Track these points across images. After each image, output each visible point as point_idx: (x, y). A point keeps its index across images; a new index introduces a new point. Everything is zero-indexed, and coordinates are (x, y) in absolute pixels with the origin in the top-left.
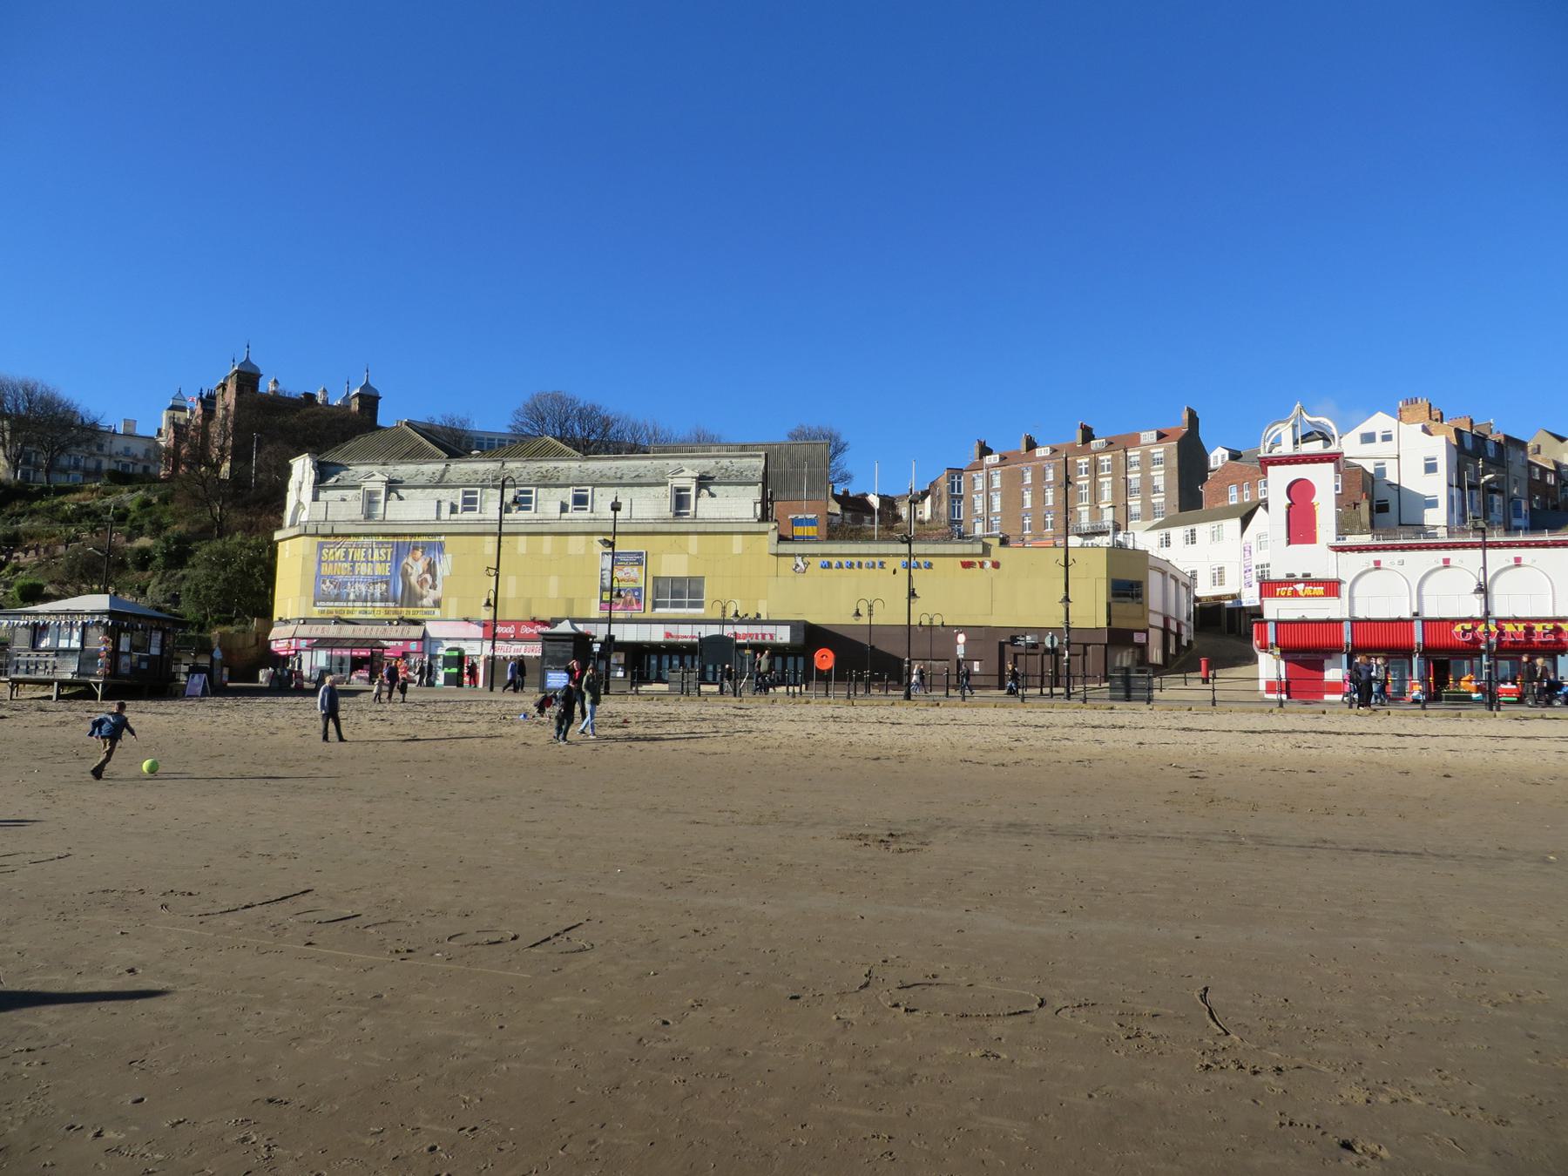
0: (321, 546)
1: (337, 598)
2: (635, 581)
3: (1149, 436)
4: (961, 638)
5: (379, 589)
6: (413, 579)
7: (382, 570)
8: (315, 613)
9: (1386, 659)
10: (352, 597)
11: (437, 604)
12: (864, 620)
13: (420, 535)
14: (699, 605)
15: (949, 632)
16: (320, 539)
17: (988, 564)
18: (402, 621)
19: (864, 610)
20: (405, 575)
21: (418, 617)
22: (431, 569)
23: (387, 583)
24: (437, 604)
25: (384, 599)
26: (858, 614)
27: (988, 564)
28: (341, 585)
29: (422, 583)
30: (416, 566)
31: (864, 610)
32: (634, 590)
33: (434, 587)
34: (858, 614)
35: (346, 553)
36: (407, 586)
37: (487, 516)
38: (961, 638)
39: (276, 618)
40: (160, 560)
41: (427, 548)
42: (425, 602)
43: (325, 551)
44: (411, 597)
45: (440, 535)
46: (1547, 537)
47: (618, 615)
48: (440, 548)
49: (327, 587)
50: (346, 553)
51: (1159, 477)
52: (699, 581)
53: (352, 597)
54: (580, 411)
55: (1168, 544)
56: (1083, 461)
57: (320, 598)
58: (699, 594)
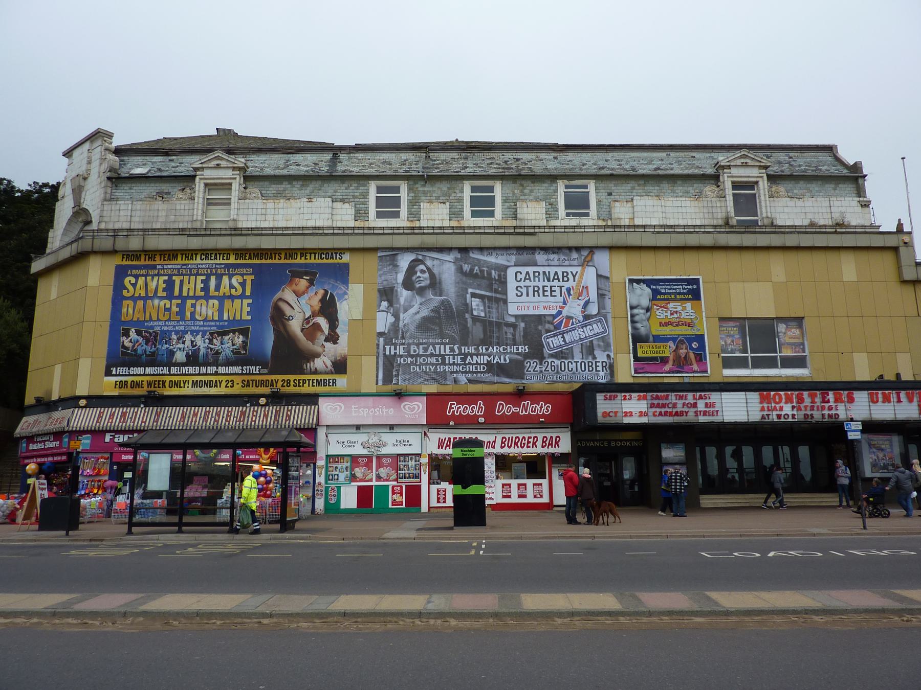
0: (121, 273)
1: (152, 360)
2: (689, 325)
4: (695, 287)
5: (230, 344)
6: (295, 326)
7: (241, 310)
8: (108, 385)
10: (180, 357)
11: (340, 366)
13: (304, 252)
16: (118, 260)
18: (277, 398)
20: (279, 318)
21: (306, 389)
22: (328, 308)
23: (244, 332)
24: (340, 366)
25: (239, 359)
28: (152, 338)
29: (312, 331)
30: (299, 304)
32: (690, 339)
33: (333, 338)
35: (170, 285)
36: (284, 339)
38: (695, 287)
39: (29, 400)
41: (311, 274)
42: (318, 363)
43: (128, 280)
44: (290, 356)
45: (341, 251)
46: (381, 363)
47: (186, 519)
48: (341, 273)
49: (131, 340)
50: (170, 285)
53: (180, 357)
57: (118, 359)
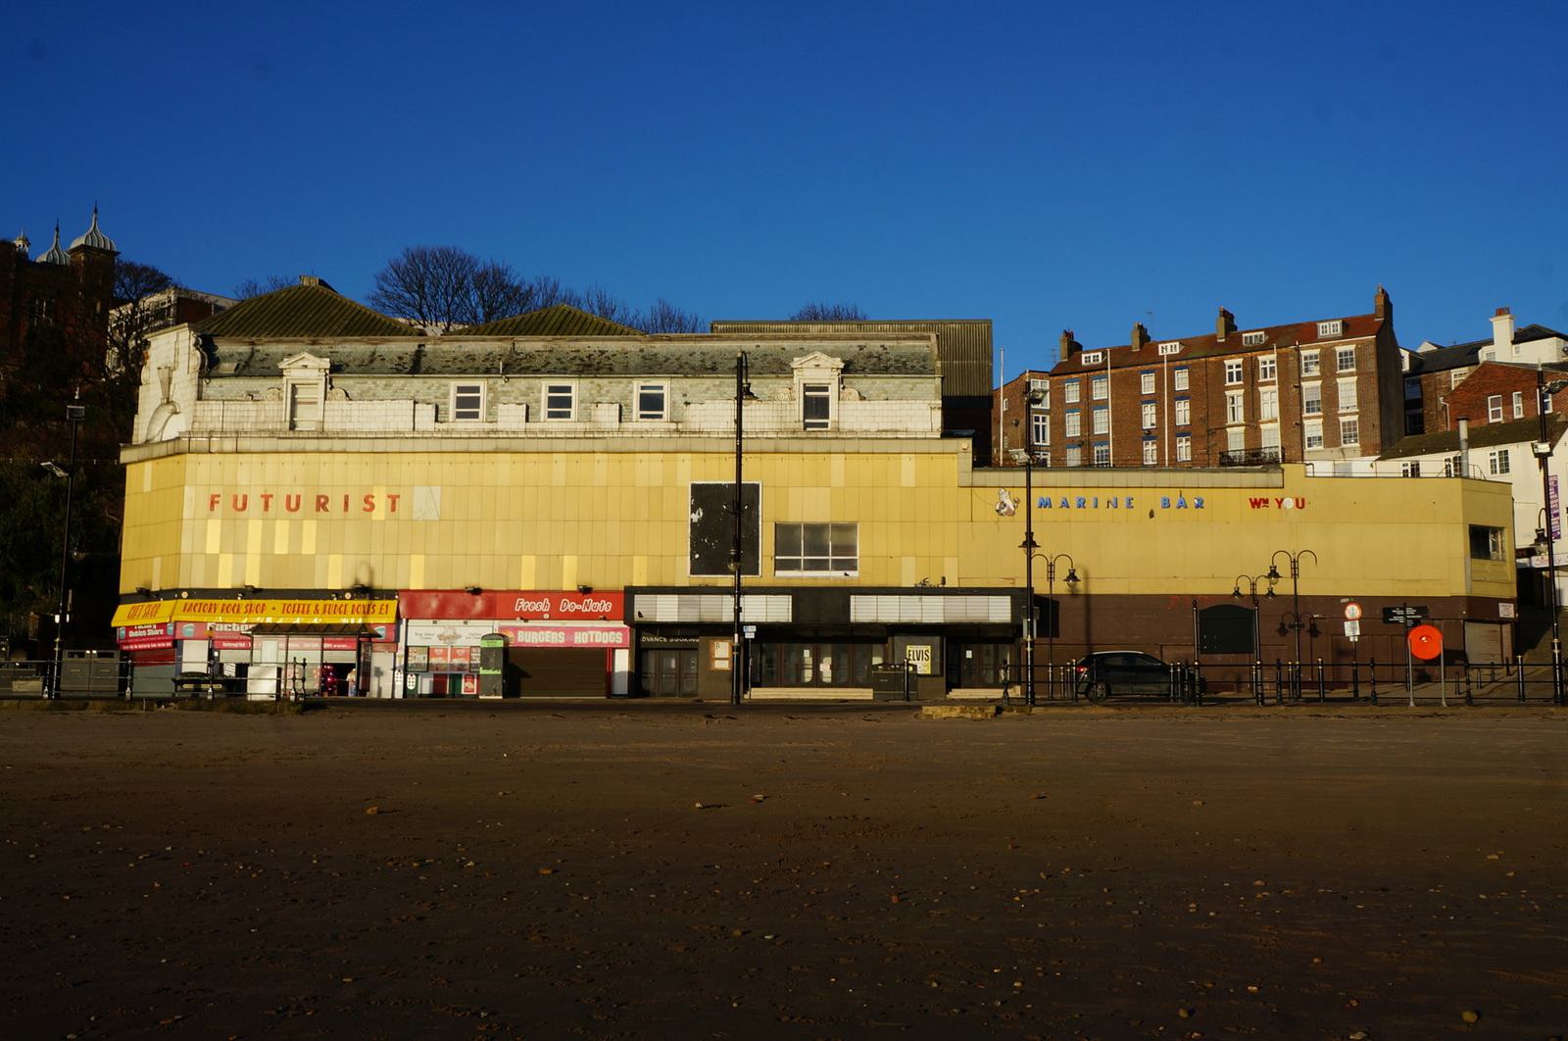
3: (1330, 328)
4: (1353, 611)
9: (566, 634)
12: (1284, 587)
14: (851, 565)
15: (1334, 605)
17: (1289, 503)
19: (1284, 569)
26: (1274, 574)
27: (1289, 503)
31: (1284, 569)
34: (1274, 574)
37: (500, 426)
38: (1353, 611)
40: (1119, 449)
51: (1348, 389)
52: (848, 529)
54: (484, 275)
55: (1505, 469)
56: (1234, 363)
58: (851, 549)
